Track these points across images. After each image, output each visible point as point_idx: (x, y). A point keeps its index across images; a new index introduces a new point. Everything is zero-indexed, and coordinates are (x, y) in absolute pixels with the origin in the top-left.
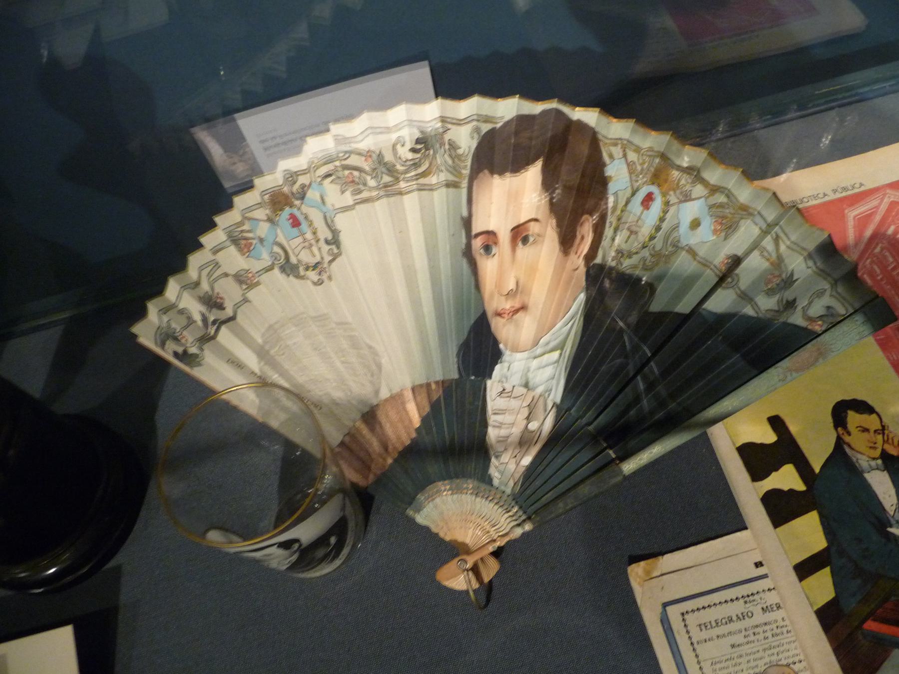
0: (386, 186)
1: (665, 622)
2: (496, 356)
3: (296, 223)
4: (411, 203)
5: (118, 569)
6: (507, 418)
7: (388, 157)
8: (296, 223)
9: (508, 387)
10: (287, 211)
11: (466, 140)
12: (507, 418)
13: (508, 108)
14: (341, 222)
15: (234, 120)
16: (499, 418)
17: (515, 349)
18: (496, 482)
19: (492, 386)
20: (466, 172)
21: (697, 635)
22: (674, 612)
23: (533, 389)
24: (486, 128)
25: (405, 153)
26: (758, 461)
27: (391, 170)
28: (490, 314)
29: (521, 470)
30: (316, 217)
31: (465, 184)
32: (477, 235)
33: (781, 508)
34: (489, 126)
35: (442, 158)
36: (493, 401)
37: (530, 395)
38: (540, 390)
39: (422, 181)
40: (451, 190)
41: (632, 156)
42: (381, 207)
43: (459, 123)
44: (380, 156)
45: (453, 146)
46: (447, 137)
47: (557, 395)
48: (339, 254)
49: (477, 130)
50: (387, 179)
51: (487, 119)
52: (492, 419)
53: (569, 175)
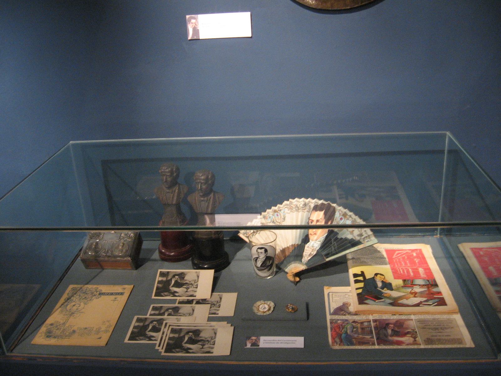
0: (297, 210)
1: (328, 294)
2: (308, 241)
3: (277, 215)
4: (300, 214)
5: (222, 272)
6: (308, 251)
7: (298, 206)
8: (277, 215)
9: (309, 246)
10: (276, 213)
11: (312, 206)
12: (308, 251)
13: (320, 202)
14: (287, 215)
15: (214, 215)
16: (306, 251)
17: (312, 240)
18: (303, 261)
19: (307, 246)
20: (311, 210)
21: (333, 296)
22: (331, 294)
23: (314, 247)
24: (316, 204)
25: (301, 205)
26: (355, 275)
27: (298, 208)
28: (309, 234)
29: (308, 260)
30: (282, 215)
31: (311, 212)
32: (310, 220)
33: (356, 282)
34: (317, 204)
35: (307, 207)
36: (306, 248)
37: (313, 248)
38: (315, 248)
39: (303, 210)
40: (308, 213)
41: (340, 212)
42: (295, 213)
43: (312, 203)
44: (297, 205)
45: (310, 206)
46: (309, 204)
47: (318, 249)
48: (284, 221)
49: (315, 204)
50: (297, 209)
51: (317, 203)
52: (305, 251)
53: (329, 213)
